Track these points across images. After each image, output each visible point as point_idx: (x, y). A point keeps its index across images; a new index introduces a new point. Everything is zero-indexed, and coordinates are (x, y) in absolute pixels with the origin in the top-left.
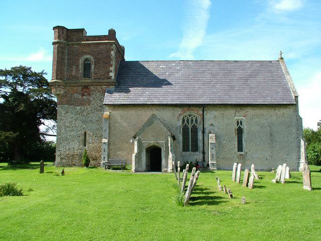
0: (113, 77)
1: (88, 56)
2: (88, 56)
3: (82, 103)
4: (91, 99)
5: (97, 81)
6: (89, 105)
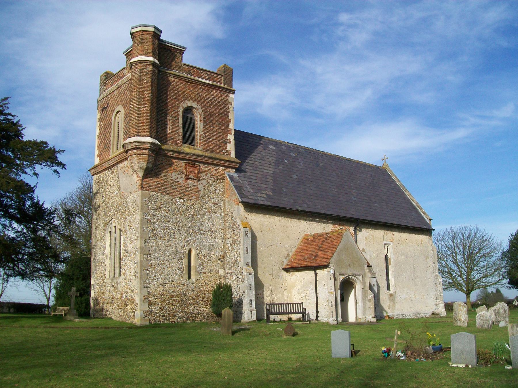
0: (233, 155)
1: (194, 105)
2: (194, 105)
3: (184, 194)
4: (200, 187)
5: (209, 154)
6: (197, 198)
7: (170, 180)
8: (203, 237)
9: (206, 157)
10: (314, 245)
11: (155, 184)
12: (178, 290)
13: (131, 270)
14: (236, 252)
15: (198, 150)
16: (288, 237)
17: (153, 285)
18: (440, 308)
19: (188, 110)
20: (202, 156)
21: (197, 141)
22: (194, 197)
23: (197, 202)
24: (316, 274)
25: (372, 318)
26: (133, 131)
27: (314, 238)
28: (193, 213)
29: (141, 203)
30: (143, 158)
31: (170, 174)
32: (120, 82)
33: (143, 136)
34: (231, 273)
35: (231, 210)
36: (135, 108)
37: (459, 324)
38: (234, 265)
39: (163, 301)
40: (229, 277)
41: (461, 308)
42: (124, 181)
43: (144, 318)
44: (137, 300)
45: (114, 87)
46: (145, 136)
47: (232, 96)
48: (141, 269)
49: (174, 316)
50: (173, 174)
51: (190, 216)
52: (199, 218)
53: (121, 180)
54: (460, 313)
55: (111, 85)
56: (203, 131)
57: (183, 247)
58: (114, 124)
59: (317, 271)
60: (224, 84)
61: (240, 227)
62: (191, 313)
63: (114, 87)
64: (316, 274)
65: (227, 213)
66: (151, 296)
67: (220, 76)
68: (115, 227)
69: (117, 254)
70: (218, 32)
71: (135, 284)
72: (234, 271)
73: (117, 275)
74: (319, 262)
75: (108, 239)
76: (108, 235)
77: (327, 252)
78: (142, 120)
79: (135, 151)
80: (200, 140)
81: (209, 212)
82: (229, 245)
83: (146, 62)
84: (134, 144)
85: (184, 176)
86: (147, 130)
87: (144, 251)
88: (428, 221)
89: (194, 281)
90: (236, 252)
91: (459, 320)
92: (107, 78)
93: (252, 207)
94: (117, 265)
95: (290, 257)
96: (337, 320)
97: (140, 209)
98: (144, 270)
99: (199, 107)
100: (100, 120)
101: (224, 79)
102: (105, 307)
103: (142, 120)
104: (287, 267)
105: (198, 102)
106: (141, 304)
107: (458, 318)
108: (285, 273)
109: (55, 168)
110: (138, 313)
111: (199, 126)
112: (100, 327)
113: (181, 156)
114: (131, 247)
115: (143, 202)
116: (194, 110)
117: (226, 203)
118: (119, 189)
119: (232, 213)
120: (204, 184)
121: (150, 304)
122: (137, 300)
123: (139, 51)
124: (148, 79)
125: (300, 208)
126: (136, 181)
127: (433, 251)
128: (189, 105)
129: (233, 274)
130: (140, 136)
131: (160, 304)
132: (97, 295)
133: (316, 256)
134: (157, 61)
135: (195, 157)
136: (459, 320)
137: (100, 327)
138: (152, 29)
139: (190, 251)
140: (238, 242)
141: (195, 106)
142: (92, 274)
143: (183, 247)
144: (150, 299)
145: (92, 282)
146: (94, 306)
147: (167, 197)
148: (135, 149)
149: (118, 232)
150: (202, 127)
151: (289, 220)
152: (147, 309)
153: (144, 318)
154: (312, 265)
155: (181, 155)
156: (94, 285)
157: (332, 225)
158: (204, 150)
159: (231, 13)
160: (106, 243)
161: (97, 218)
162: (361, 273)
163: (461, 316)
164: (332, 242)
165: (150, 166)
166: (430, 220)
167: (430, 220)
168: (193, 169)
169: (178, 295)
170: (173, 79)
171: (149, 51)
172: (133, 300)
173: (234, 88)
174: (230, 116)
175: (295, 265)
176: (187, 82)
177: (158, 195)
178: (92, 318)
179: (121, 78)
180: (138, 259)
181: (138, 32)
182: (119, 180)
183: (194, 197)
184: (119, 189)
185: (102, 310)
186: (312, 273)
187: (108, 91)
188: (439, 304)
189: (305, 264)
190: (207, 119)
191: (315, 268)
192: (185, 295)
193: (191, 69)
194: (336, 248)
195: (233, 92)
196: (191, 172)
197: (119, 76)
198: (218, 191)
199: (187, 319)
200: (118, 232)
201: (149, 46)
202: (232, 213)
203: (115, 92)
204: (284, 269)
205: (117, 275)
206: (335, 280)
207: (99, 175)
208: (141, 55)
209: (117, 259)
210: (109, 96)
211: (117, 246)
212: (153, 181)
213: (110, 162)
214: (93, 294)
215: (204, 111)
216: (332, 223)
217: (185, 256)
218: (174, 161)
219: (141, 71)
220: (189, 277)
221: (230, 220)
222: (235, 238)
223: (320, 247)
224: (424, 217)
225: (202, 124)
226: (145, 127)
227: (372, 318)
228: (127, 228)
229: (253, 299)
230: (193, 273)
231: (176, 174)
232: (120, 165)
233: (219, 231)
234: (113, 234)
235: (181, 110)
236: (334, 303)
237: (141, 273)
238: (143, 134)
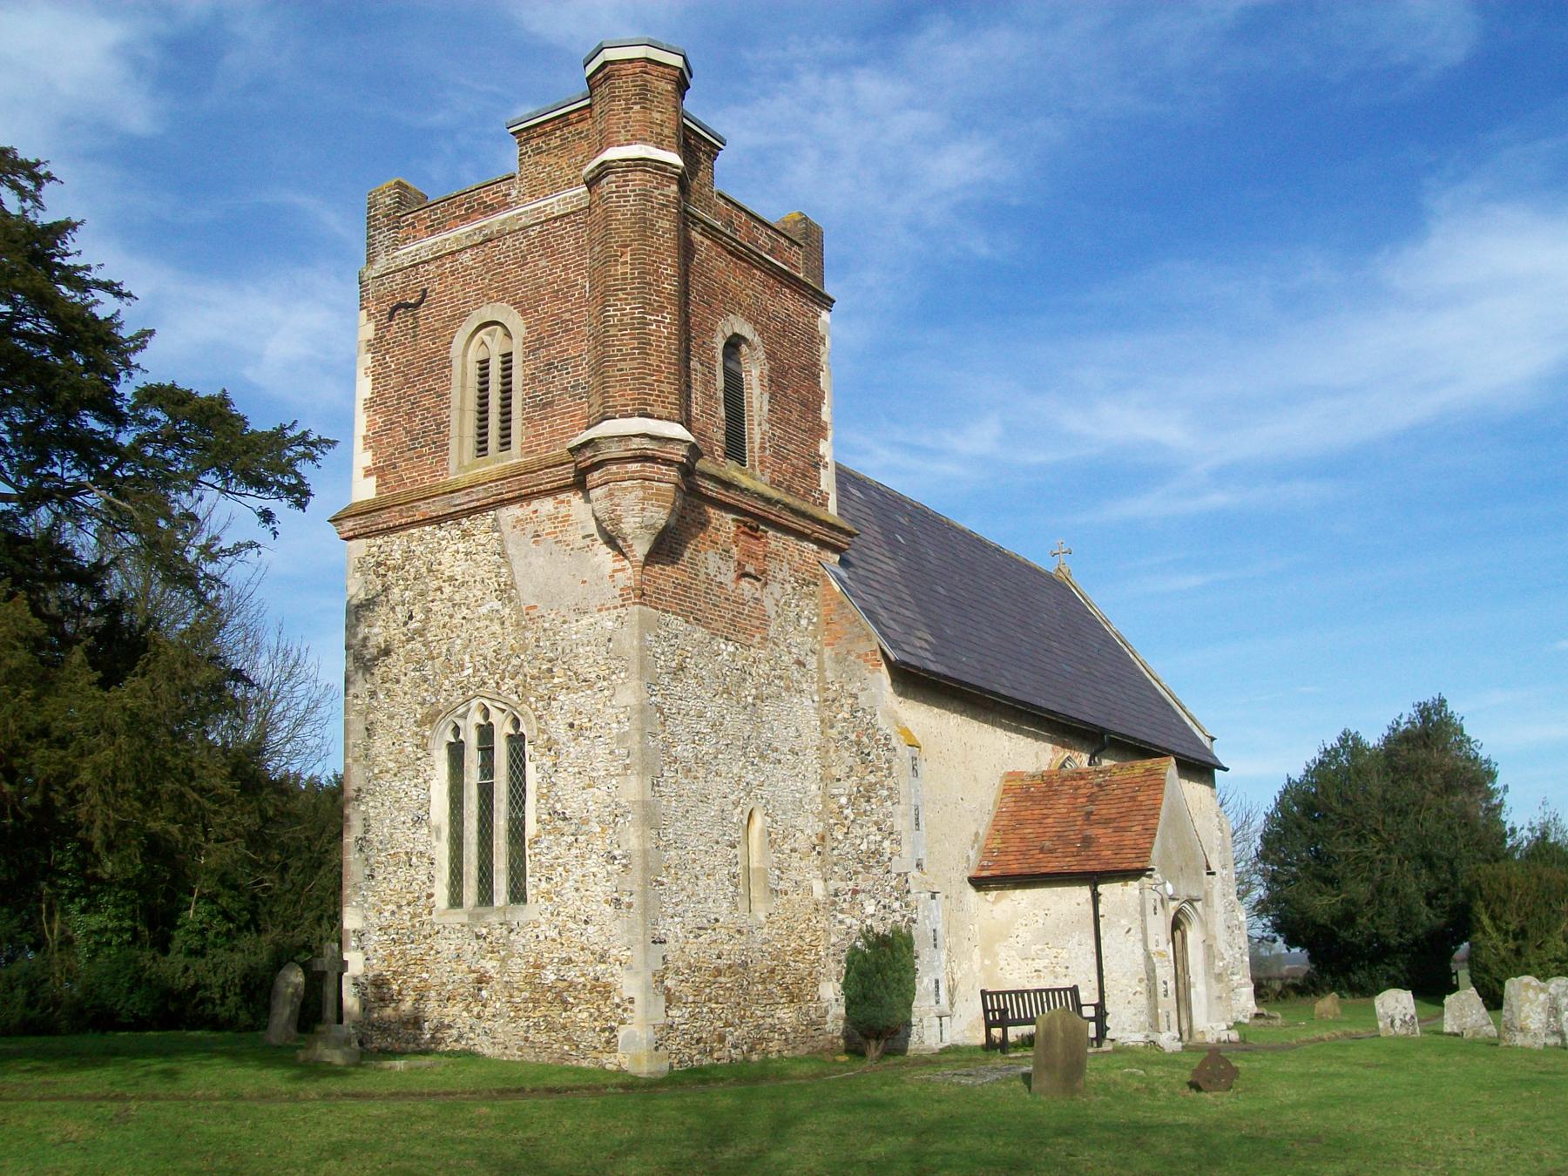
1: (746, 330)
7: (702, 577)
8: (780, 771)
9: (786, 506)
10: (1062, 806)
11: (669, 587)
14: (876, 823)
16: (975, 779)
17: (672, 929)
18: (1243, 999)
19: (734, 344)
20: (778, 502)
21: (751, 451)
22: (758, 638)
23: (763, 654)
24: (1096, 897)
25: (1229, 1028)
26: (622, 395)
27: (1049, 784)
28: (754, 691)
29: (641, 649)
30: (659, 494)
31: (702, 556)
32: (495, 221)
33: (659, 418)
34: (855, 892)
35: (853, 688)
36: (627, 320)
37: (1519, 1040)
38: (868, 868)
39: (698, 991)
40: (845, 906)
41: (1531, 994)
42: (536, 569)
43: (656, 1049)
46: (668, 419)
47: (825, 316)
48: (644, 879)
49: (722, 1039)
50: (711, 552)
51: (750, 699)
52: (767, 709)
53: (518, 566)
54: (1526, 1008)
55: (433, 230)
56: (769, 421)
57: (736, 804)
58: (464, 366)
59: (1101, 888)
60: (807, 273)
61: (894, 743)
62: (758, 1026)
64: (1096, 897)
65: (831, 695)
66: (670, 974)
67: (795, 248)
70: (138, 116)
72: (862, 886)
74: (1107, 857)
77: (1124, 829)
78: (653, 361)
79: (634, 466)
80: (763, 448)
81: (788, 689)
82: (844, 800)
83: (661, 166)
84: (636, 443)
85: (732, 565)
86: (672, 398)
88: (1206, 742)
89: (764, 920)
90: (876, 823)
91: (1522, 1030)
93: (914, 681)
95: (982, 842)
96: (1180, 1039)
97: (635, 668)
98: (651, 881)
99: (757, 340)
101: (806, 258)
102: (432, 1008)
103: (653, 361)
104: (985, 874)
105: (756, 323)
106: (648, 1003)
107: (1517, 1024)
108: (971, 891)
109: (266, 504)
112: (528, 1087)
113: (730, 497)
115: (644, 648)
116: (744, 348)
117: (828, 664)
118: (506, 592)
119: (855, 697)
120: (777, 596)
121: (670, 999)
123: (635, 127)
124: (667, 225)
126: (608, 571)
127: (1221, 830)
128: (737, 331)
129: (860, 897)
130: (651, 416)
131: (691, 999)
132: (378, 967)
133: (1087, 841)
135: (760, 504)
136: (1522, 1030)
137: (528, 1087)
138: (677, 61)
140: (885, 793)
141: (749, 336)
142: (347, 891)
143: (736, 804)
144: (668, 983)
145: (351, 920)
146: (365, 1007)
147: (700, 634)
148: (635, 459)
150: (766, 407)
151: (975, 724)
152: (661, 1020)
153: (656, 1049)
154: (1088, 868)
155: (732, 493)
156: (360, 935)
157: (1050, 746)
158: (775, 484)
159: (183, 59)
160: (434, 784)
161: (373, 694)
162: (1201, 895)
163: (1527, 1017)
164: (1133, 799)
165: (673, 522)
166: (1213, 739)
167: (1213, 739)
168: (757, 547)
169: (730, 967)
170: (700, 238)
171: (666, 132)
173: (829, 289)
174: (825, 381)
175: (1015, 868)
176: (730, 253)
177: (677, 623)
178: (274, 1056)
179: (491, 209)
181: (631, 61)
182: (508, 564)
183: (758, 638)
184: (506, 592)
185: (416, 1021)
186: (1084, 892)
188: (1242, 986)
189: (1053, 866)
190: (776, 382)
191: (1093, 879)
192: (744, 965)
194: (1156, 816)
195: (827, 302)
198: (804, 622)
199: (751, 1050)
202: (855, 697)
203: (466, 257)
207: (379, 541)
208: (644, 141)
210: (432, 267)
212: (666, 575)
213: (460, 499)
214: (355, 963)
215: (771, 356)
216: (1052, 742)
218: (711, 511)
219: (645, 196)
221: (845, 720)
222: (872, 778)
223: (1091, 813)
224: (1195, 729)
225: (766, 396)
226: (666, 388)
227: (1229, 1028)
231: (716, 553)
232: (515, 511)
233: (811, 754)
235: (720, 343)
237: (645, 892)
238: (658, 410)
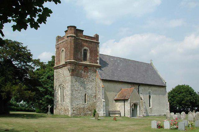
12: (82, 106)
13: (68, 100)
15: (87, 63)
44: (70, 109)
45: (61, 41)
63: (61, 41)
68: (62, 86)
69: (63, 95)
71: (69, 105)
73: (63, 101)
75: (60, 90)
76: (60, 89)
87: (72, 95)
92: (59, 38)
94: (63, 98)
98: (72, 102)
100: (56, 51)
110: (70, 113)
111: (88, 55)
114: (68, 93)
121: (74, 110)
122: (70, 109)
125: (120, 81)
134: (75, 36)
139: (86, 94)
149: (63, 88)
167: (166, 83)
172: (68, 109)
173: (99, 42)
180: (70, 97)
187: (59, 42)
190: (91, 53)
193: (86, 37)
196: (86, 70)
197: (63, 38)
200: (63, 88)
201: (73, 31)
204: (114, 100)
205: (63, 101)
206: (130, 104)
209: (63, 96)
211: (62, 93)
217: (84, 96)
220: (85, 102)
228: (66, 87)
229: (105, 109)
230: (86, 101)
234: (61, 89)
236: (130, 111)
